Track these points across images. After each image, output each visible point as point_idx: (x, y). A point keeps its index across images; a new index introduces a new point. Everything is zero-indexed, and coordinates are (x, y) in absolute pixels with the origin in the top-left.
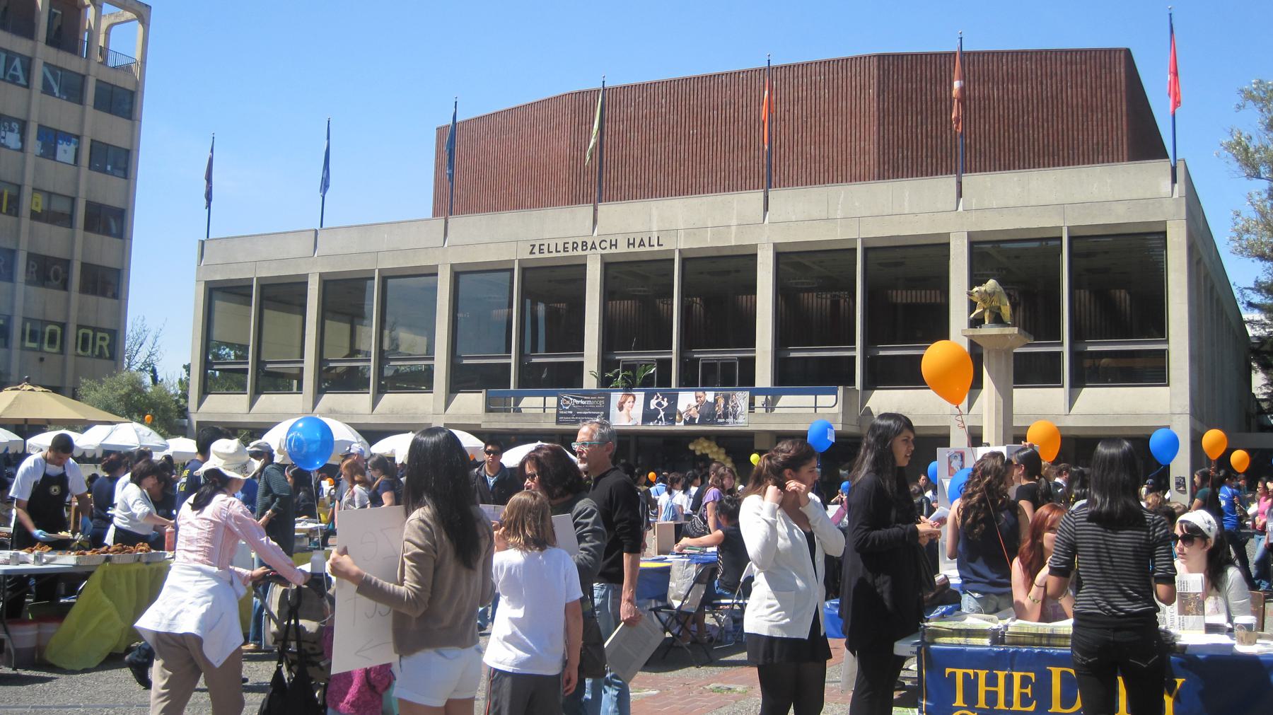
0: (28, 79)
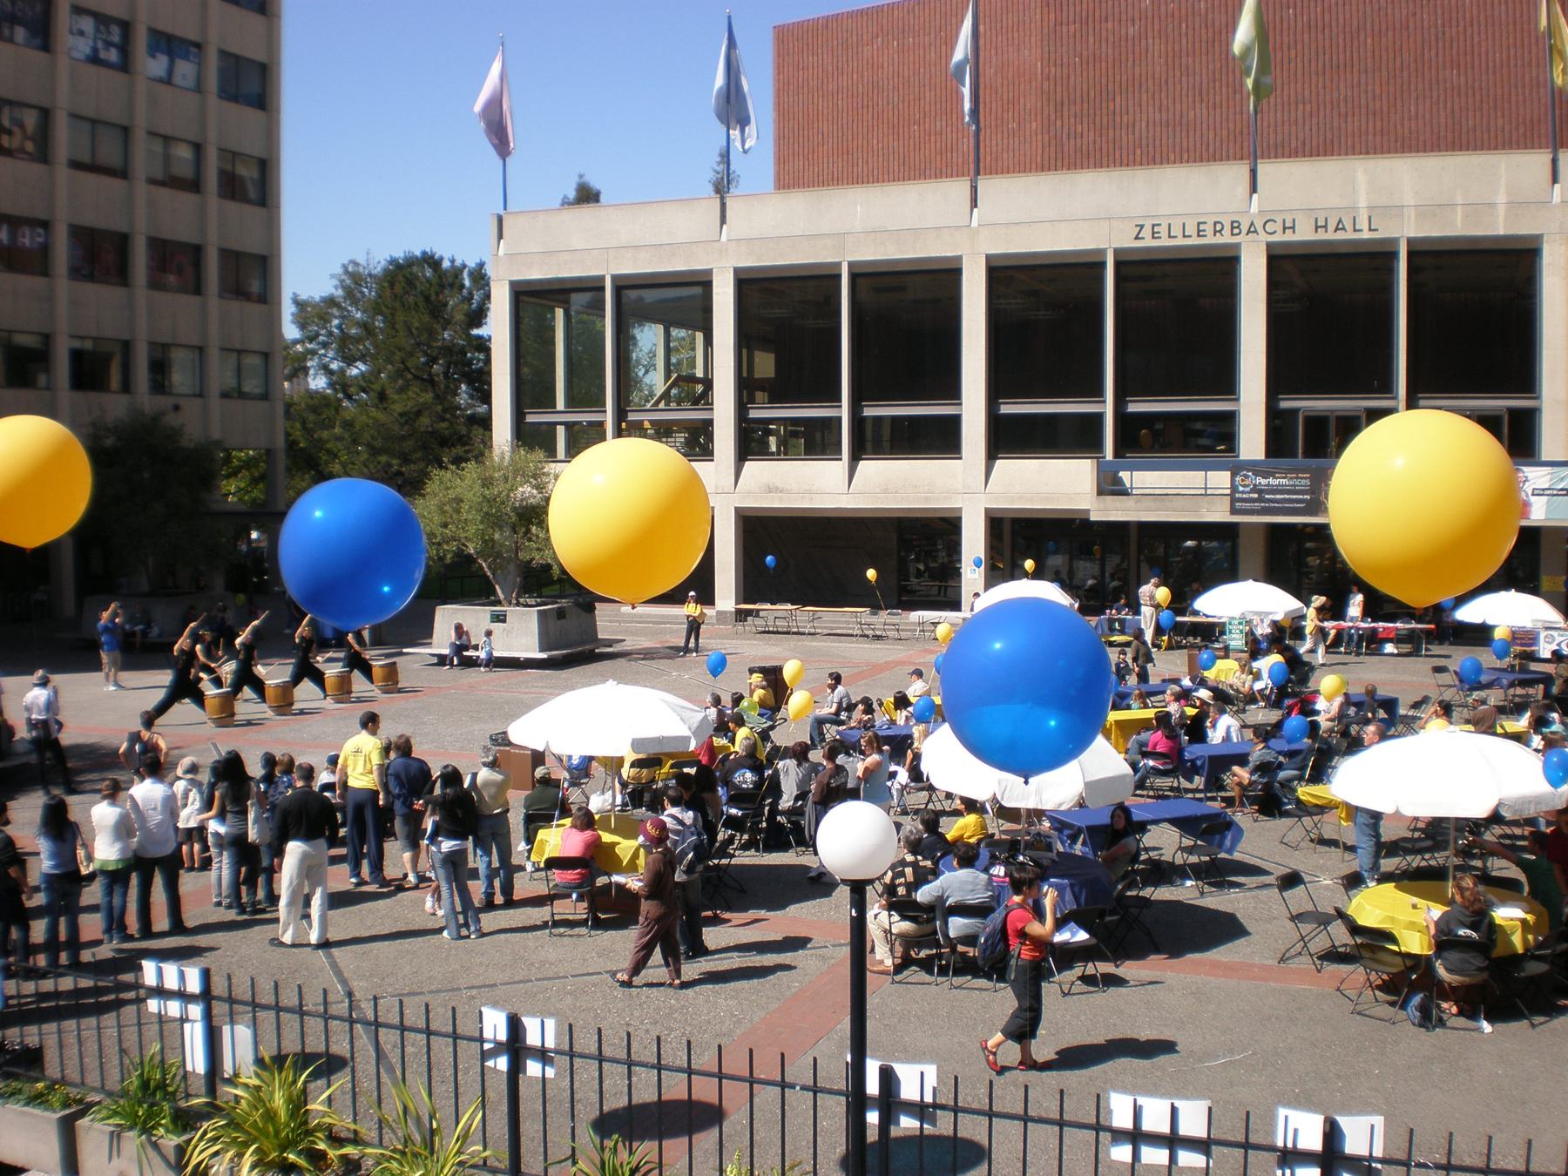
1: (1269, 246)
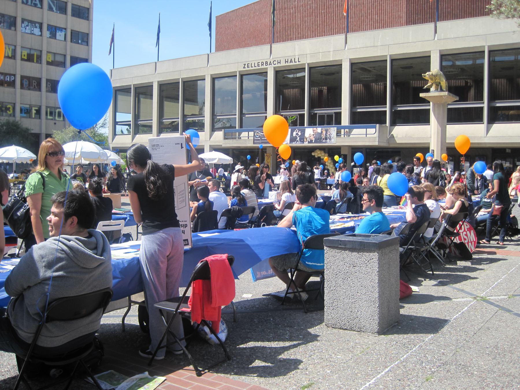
0: (42, 5)
1: (274, 67)
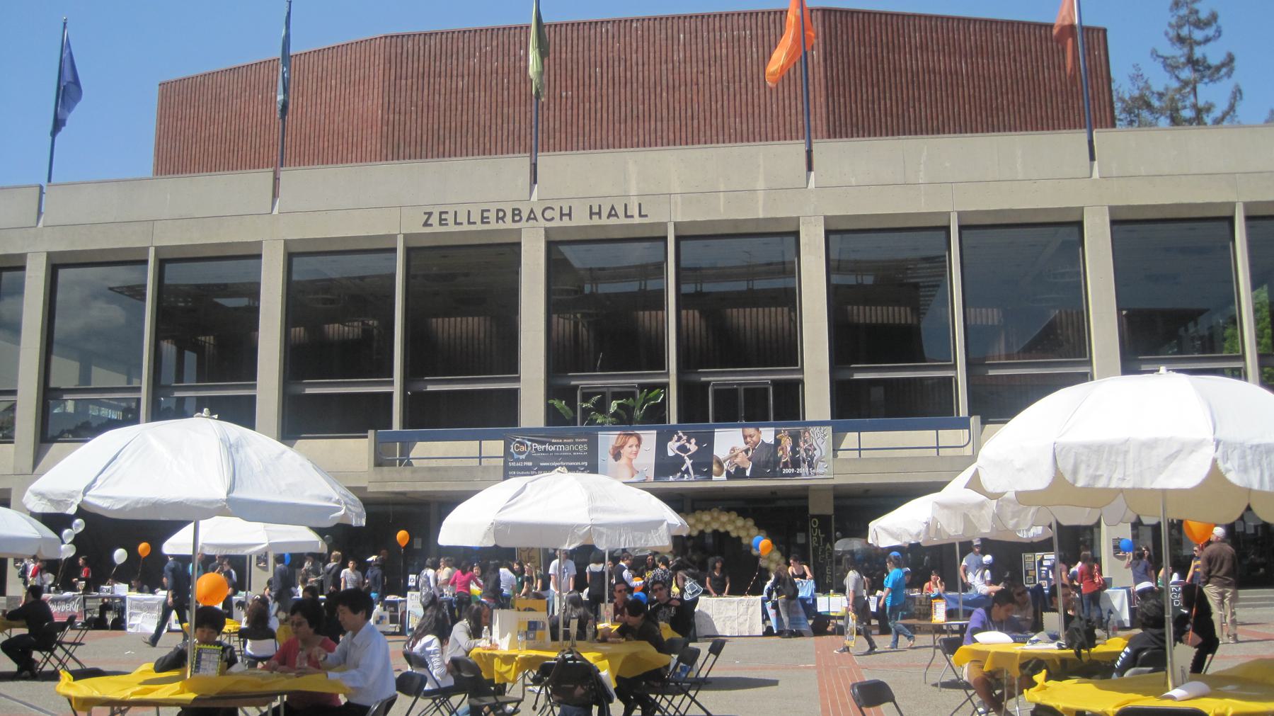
1: (547, 230)
